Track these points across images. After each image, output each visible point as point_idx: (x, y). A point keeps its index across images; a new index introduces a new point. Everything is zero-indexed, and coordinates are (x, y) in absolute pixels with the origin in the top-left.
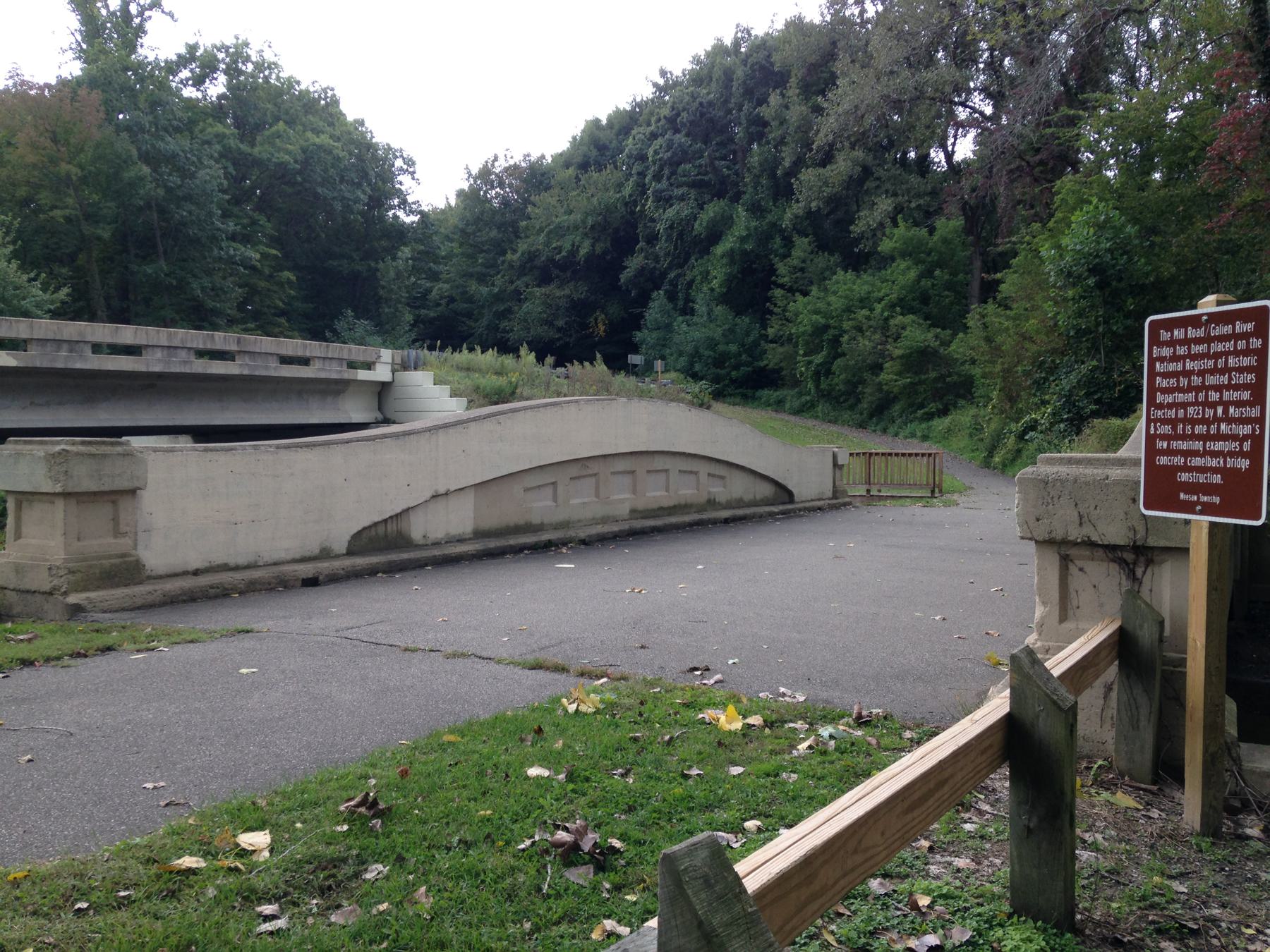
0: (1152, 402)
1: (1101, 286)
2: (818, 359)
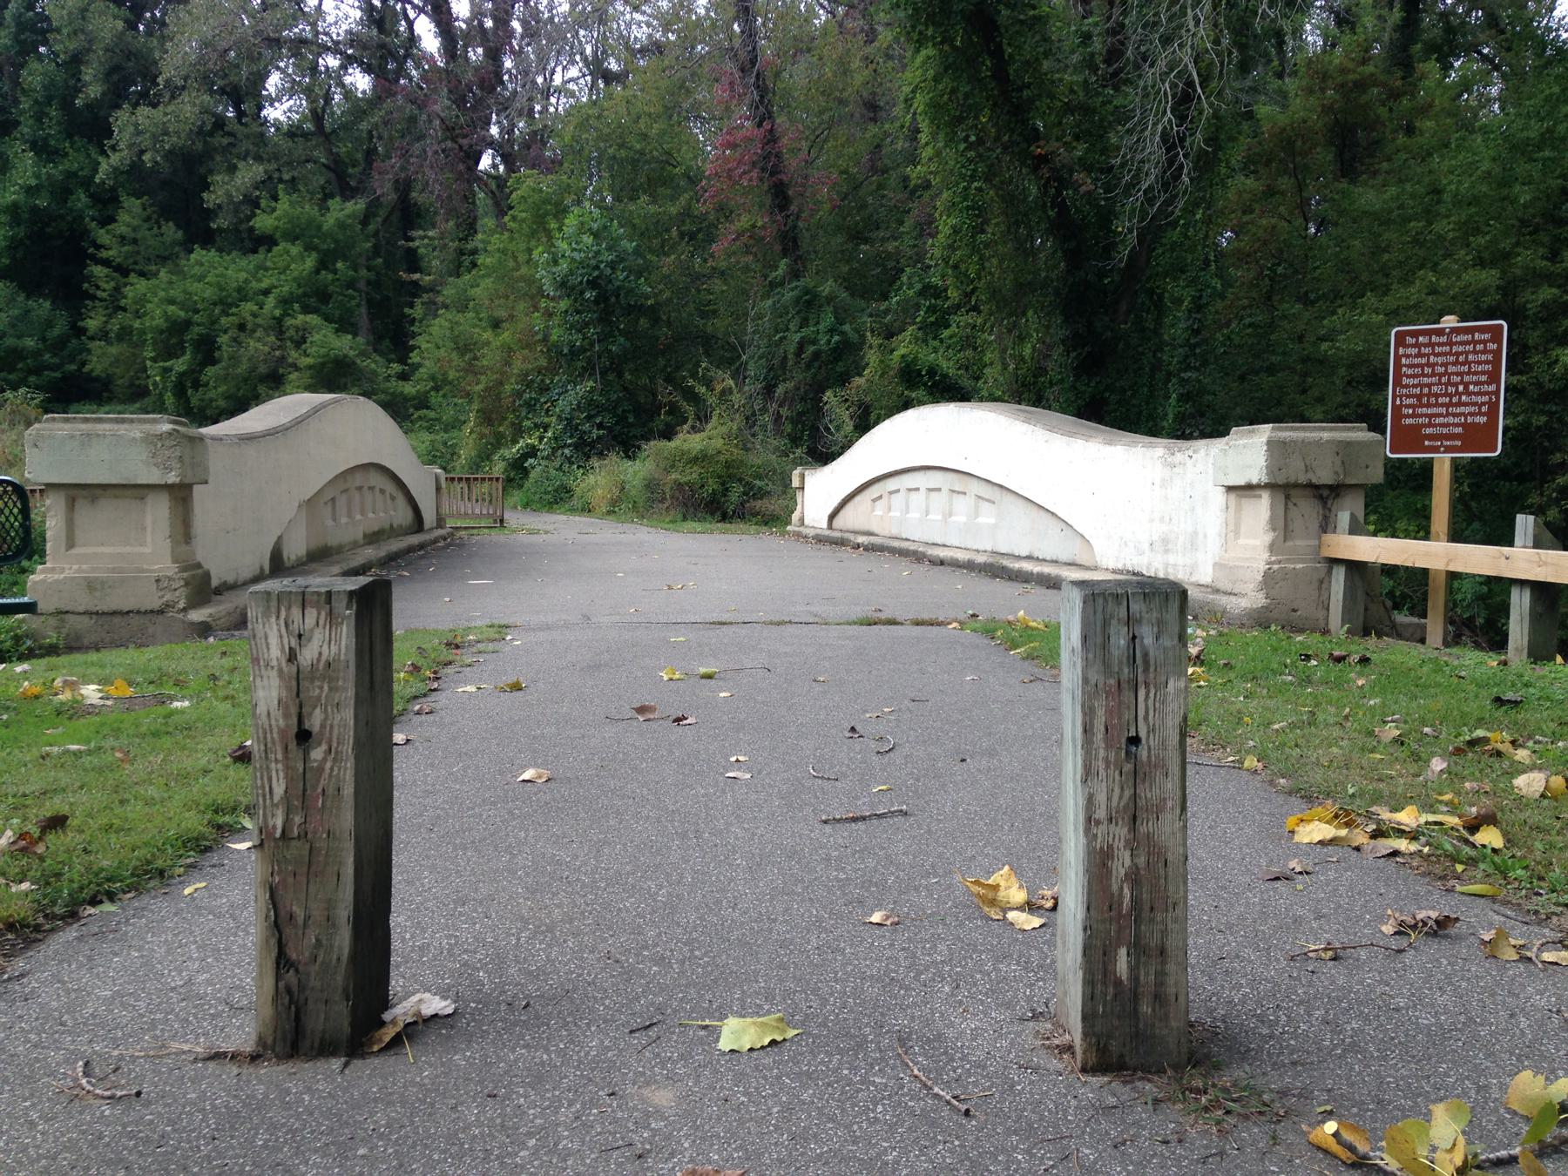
0: (1397, 383)
1: (602, 298)
2: (180, 365)
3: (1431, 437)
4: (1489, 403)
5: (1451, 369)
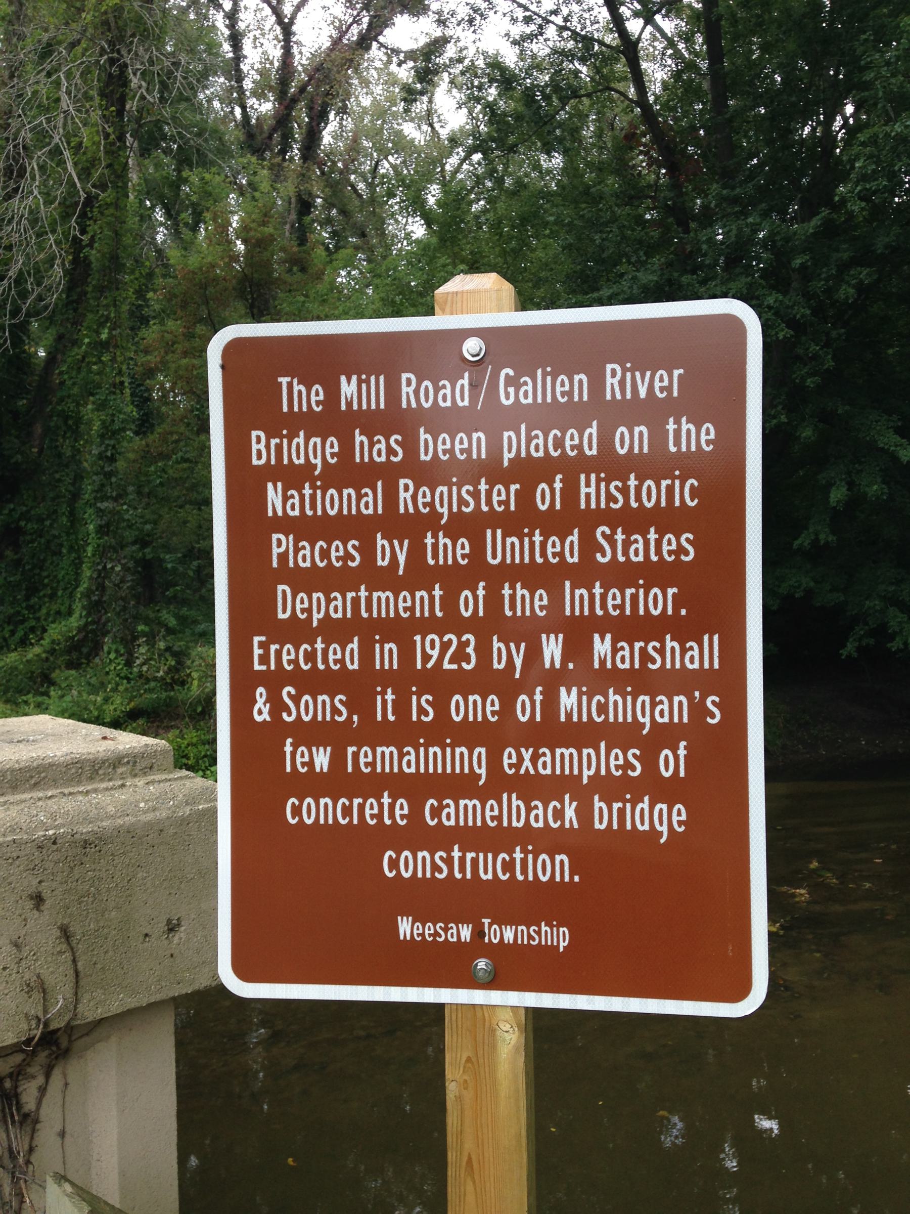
0: (252, 615)
3: (429, 899)
4: (695, 729)
5: (501, 548)
